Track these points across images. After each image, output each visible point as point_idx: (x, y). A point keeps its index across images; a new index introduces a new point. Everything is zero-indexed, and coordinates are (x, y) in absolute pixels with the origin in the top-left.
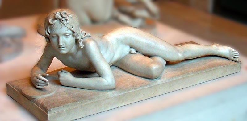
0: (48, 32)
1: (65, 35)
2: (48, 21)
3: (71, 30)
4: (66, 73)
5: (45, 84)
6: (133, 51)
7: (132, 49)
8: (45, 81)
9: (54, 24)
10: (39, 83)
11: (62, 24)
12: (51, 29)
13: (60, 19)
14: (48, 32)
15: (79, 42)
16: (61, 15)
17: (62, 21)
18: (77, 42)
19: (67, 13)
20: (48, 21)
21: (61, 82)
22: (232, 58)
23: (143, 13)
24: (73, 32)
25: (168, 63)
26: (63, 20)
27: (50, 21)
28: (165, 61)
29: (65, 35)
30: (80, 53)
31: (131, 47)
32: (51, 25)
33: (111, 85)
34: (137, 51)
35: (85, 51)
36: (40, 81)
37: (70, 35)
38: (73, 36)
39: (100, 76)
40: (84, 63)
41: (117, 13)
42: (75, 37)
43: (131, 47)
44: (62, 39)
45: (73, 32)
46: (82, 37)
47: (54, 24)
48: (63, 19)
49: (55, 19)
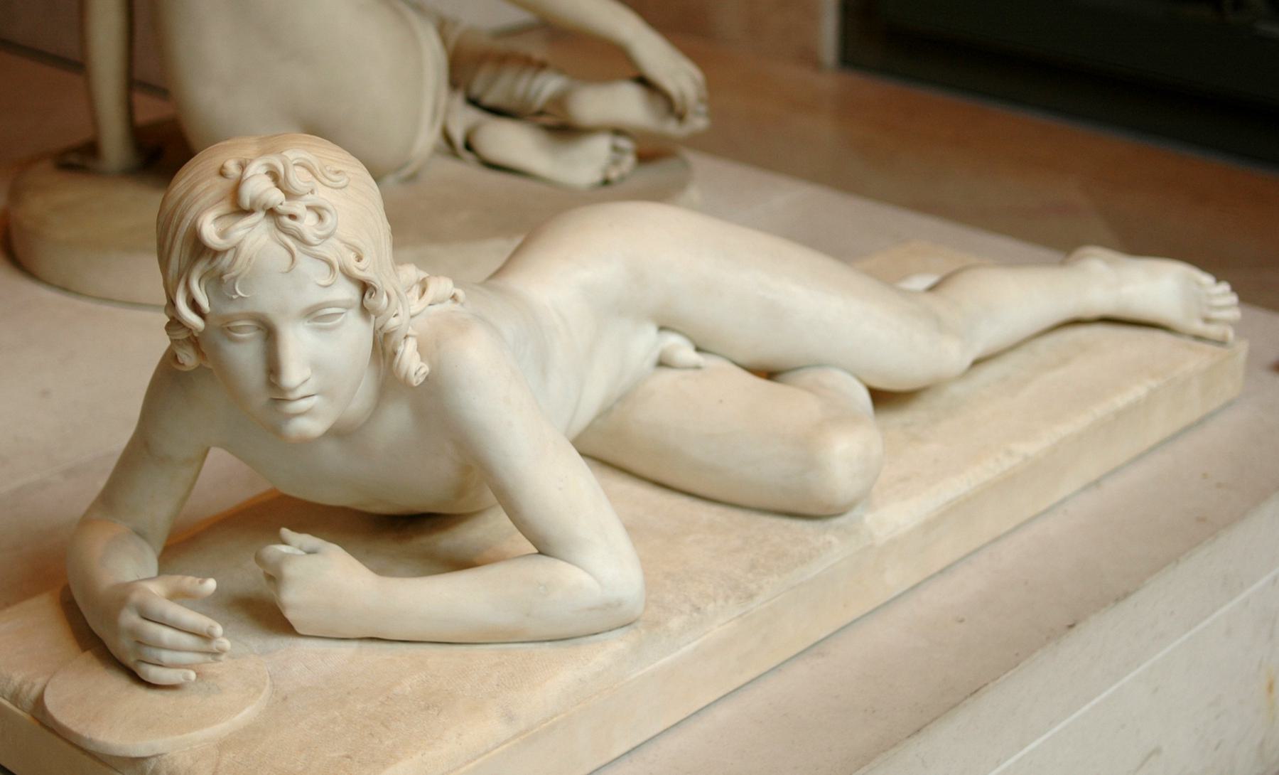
0: (194, 306)
1: (314, 314)
2: (186, 225)
3: (349, 276)
4: (311, 552)
5: (207, 653)
6: (686, 353)
7: (673, 340)
8: (206, 637)
9: (236, 248)
10: (161, 646)
11: (289, 241)
12: (217, 281)
13: (272, 212)
14: (194, 306)
15: (396, 344)
16: (274, 175)
17: (286, 220)
18: (383, 349)
19: (316, 163)
20: (186, 225)
21: (290, 615)
22: (1199, 327)
23: (622, 104)
24: (365, 287)
25: (882, 398)
26: (292, 217)
27: (210, 231)
28: (860, 380)
29: (314, 314)
30: (397, 418)
31: (662, 328)
32: (216, 253)
33: (620, 604)
34: (702, 346)
35: (434, 405)
36: (167, 634)
37: (347, 308)
38: (365, 311)
39: (540, 553)
40: (422, 484)
41: (462, 119)
42: (373, 317)
43: (662, 328)
44: (302, 351)
45: (365, 287)
46: (413, 312)
47: (236, 248)
48: (298, 207)
49: (240, 210)
